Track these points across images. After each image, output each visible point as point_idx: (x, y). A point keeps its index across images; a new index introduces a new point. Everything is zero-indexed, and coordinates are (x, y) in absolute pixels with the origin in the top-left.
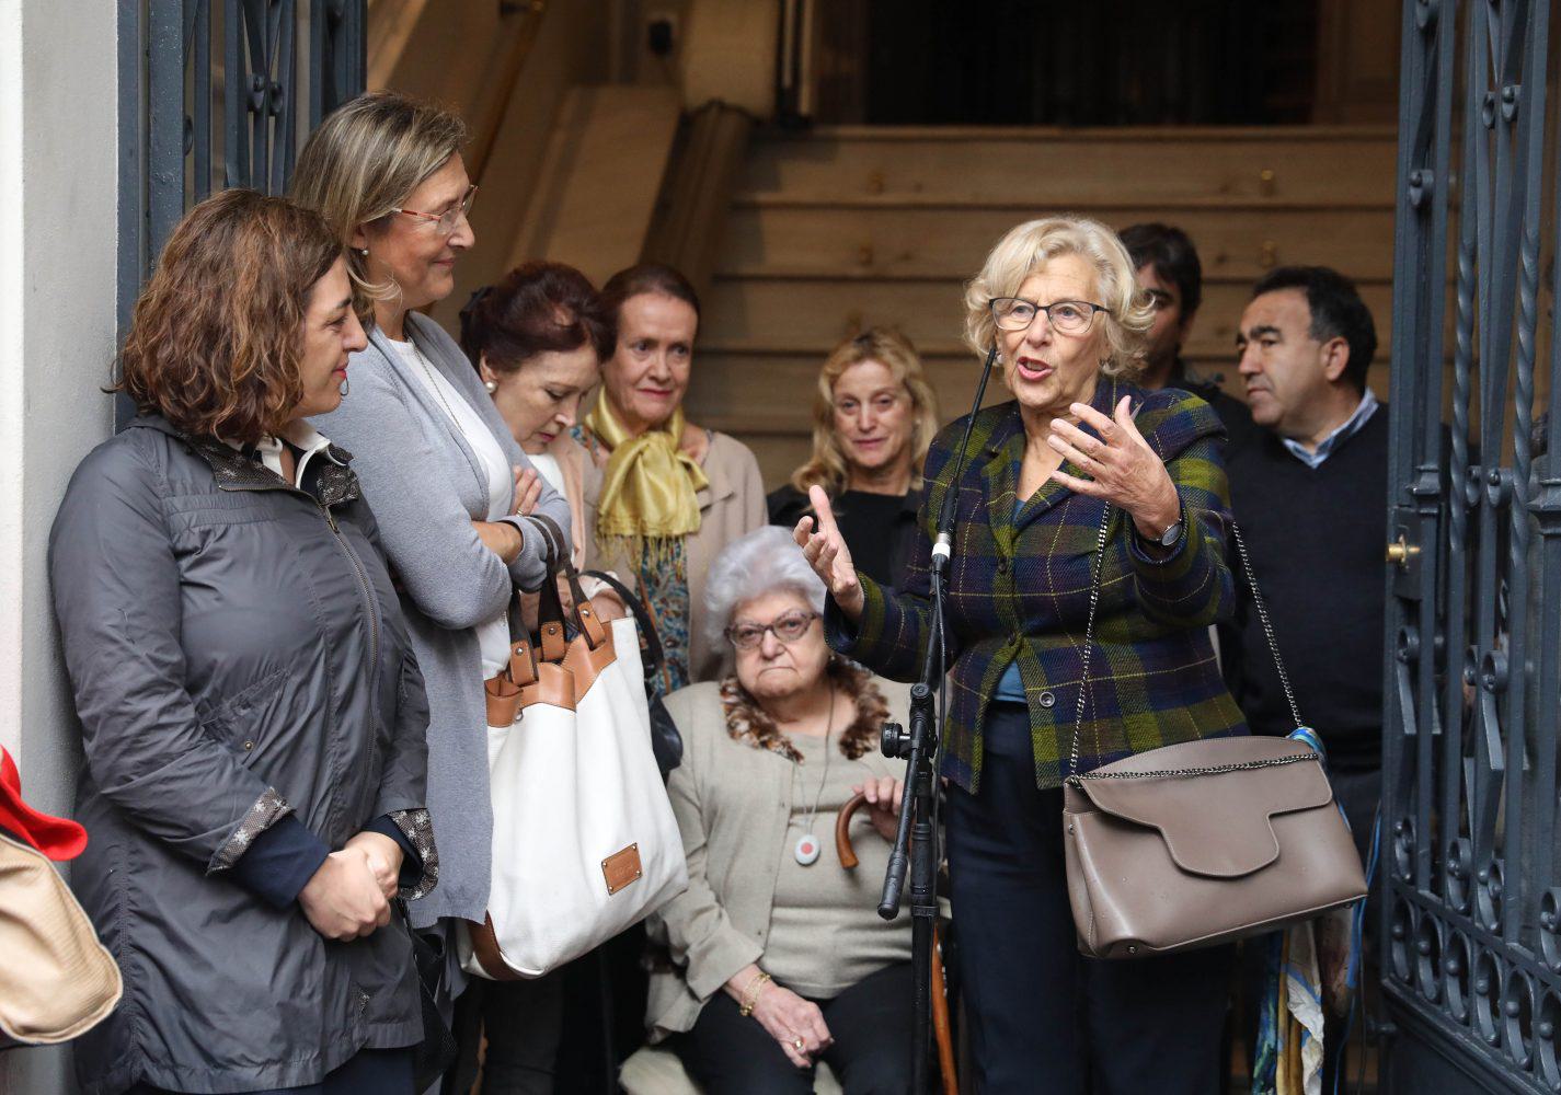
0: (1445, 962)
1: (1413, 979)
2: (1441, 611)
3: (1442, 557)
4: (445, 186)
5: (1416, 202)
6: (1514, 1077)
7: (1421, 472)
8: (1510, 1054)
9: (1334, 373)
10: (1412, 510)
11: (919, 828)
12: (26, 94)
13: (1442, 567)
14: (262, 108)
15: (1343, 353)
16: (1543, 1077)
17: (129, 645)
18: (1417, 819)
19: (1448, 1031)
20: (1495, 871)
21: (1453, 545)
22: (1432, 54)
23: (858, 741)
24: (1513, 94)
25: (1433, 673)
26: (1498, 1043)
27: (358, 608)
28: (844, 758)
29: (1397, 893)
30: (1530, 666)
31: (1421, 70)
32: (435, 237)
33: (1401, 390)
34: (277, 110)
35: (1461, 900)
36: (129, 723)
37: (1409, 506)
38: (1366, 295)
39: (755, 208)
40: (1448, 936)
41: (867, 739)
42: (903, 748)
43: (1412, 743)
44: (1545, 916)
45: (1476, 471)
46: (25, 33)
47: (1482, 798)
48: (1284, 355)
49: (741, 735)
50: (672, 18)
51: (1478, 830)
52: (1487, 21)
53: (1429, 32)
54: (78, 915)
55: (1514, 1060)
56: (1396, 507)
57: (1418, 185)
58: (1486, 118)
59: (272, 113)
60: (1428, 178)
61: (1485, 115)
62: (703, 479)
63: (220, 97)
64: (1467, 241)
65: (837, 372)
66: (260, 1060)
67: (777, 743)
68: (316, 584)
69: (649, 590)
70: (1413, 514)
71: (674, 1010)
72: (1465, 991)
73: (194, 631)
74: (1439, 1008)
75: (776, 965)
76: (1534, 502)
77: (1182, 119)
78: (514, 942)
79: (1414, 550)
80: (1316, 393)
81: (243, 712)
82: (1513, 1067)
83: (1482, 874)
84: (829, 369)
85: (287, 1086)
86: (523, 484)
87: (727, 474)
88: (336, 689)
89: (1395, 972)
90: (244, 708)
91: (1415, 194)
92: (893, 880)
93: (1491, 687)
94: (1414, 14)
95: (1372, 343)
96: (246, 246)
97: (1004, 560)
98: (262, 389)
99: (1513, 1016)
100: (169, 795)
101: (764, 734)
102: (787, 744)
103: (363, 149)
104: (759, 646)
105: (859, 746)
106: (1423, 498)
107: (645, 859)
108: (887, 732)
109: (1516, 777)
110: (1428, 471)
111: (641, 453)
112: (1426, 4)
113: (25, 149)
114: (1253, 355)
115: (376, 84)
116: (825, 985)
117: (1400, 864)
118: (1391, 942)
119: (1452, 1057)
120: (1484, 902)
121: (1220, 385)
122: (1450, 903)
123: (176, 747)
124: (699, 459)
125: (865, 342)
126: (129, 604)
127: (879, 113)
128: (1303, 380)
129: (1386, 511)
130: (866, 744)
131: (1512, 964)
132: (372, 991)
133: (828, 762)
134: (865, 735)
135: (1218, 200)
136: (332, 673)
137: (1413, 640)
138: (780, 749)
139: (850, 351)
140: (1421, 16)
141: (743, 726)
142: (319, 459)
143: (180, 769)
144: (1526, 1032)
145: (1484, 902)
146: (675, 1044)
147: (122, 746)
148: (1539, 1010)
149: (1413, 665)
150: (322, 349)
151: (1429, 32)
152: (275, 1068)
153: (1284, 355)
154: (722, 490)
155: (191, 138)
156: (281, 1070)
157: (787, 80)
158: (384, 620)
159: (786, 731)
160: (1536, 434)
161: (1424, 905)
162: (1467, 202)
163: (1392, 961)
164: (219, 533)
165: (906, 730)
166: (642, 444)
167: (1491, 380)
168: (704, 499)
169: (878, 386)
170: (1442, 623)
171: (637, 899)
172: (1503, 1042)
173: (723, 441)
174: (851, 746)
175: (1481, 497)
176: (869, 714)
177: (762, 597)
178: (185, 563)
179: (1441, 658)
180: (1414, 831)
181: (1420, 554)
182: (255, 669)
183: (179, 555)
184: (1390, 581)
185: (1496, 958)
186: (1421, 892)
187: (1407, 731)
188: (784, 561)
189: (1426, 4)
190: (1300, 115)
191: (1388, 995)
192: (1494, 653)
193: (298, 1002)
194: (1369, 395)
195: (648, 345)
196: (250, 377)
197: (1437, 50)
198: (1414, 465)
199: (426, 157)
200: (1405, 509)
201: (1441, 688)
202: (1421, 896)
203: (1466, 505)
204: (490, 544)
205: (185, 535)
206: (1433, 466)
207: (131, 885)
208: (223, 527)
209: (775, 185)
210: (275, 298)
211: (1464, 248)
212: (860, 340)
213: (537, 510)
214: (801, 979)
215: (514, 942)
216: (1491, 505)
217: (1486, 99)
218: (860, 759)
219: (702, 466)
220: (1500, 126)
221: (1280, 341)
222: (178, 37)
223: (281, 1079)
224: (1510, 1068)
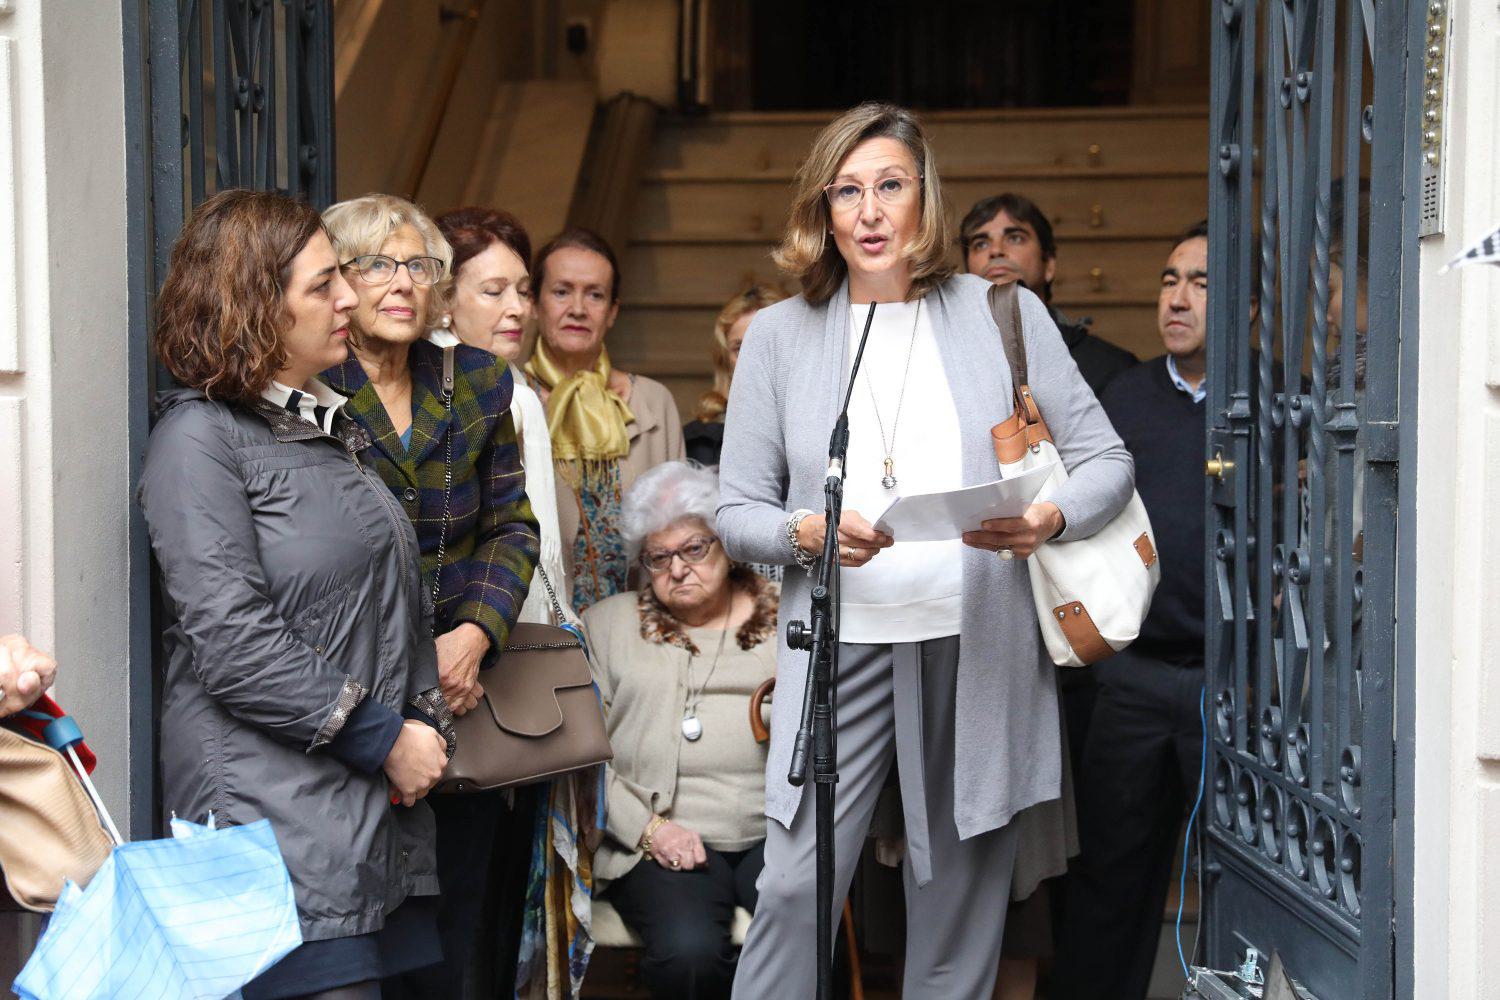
0: (1261, 811)
2: (1252, 515)
3: (1253, 469)
5: (1226, 172)
6: (1320, 905)
7: (1234, 399)
8: (1317, 886)
10: (1227, 432)
11: (820, 708)
12: (47, 99)
13: (1252, 479)
14: (247, 107)
16: (1345, 905)
17: (229, 570)
18: (1235, 690)
19: (1264, 868)
20: (1301, 733)
21: (1262, 460)
22: (1237, 45)
23: (751, 634)
24: (1306, 79)
25: (1249, 572)
26: (1306, 878)
27: (392, 534)
28: (739, 649)
29: (1219, 753)
31: (1228, 60)
33: (1215, 330)
34: (260, 108)
35: (1274, 758)
36: (237, 634)
37: (1224, 428)
39: (664, 183)
40: (1263, 789)
41: (759, 633)
42: (806, 641)
43: (1230, 627)
44: (1344, 770)
45: (1280, 397)
46: (44, 46)
47: (1290, 673)
49: (651, 634)
50: (587, 22)
51: (1287, 699)
52: (1283, 18)
53: (1234, 29)
54: (77, 790)
55: (1320, 891)
56: (1213, 429)
57: (1227, 157)
58: (1283, 100)
59: (255, 110)
61: (1283, 98)
62: (630, 415)
65: (730, 322)
66: (343, 911)
67: (678, 639)
68: (361, 515)
69: (592, 510)
70: (1228, 434)
73: (269, 557)
74: (1256, 850)
76: (1330, 423)
77: (1020, 102)
79: (1229, 465)
81: (314, 622)
82: (1320, 897)
83: (1291, 736)
84: (723, 320)
85: (364, 932)
87: (650, 407)
88: (381, 600)
89: (1219, 820)
90: (314, 619)
91: (1225, 165)
92: (800, 753)
93: (1296, 579)
94: (1221, 12)
99: (1319, 854)
100: (276, 688)
104: (669, 569)
105: (752, 638)
106: (1237, 421)
108: (792, 628)
109: (1319, 656)
110: (1240, 398)
111: (577, 389)
112: (1231, 4)
113: (46, 146)
117: (1222, 729)
118: (1214, 795)
119: (1268, 890)
121: (1088, 327)
122: (1264, 761)
123: (277, 649)
124: (626, 398)
125: (752, 296)
126: (223, 538)
127: (762, 104)
129: (1204, 432)
130: (758, 637)
131: (1317, 811)
132: (409, 849)
133: (721, 651)
134: (757, 629)
135: (1056, 171)
136: (377, 587)
137: (1229, 541)
138: (680, 643)
139: (740, 304)
140: (1227, 14)
141: (652, 627)
143: (283, 665)
144: (1330, 867)
145: (1293, 759)
147: (234, 653)
148: (1341, 850)
149: (1230, 562)
151: (1234, 29)
152: (354, 918)
155: (188, 134)
156: (359, 920)
157: (687, 74)
158: (409, 543)
161: (1242, 763)
162: (1268, 169)
163: (1216, 811)
164: (282, 477)
165: (808, 625)
166: (577, 382)
167: (1292, 320)
168: (632, 431)
170: (1254, 527)
172: (1311, 874)
173: (644, 383)
176: (763, 612)
177: (669, 529)
178: (256, 501)
179: (1253, 555)
180: (1233, 702)
181: (1233, 469)
182: (324, 586)
183: (251, 495)
184: (1209, 491)
185: (1304, 806)
186: (1239, 752)
187: (1226, 617)
188: (684, 496)
189: (1231, 4)
190: (1120, 97)
191: (1212, 837)
192: (1298, 551)
193: (372, 864)
195: (568, 287)
197: (1241, 44)
198: (1227, 393)
200: (1220, 431)
202: (1240, 756)
203: (1272, 426)
205: (255, 480)
206: (1244, 394)
208: (284, 472)
209: (678, 164)
210: (254, 276)
211: (1267, 210)
212: (748, 295)
214: (715, 838)
216: (1294, 427)
217: (1283, 83)
218: (752, 650)
219: (628, 403)
220: (1296, 107)
222: (174, 47)
223: (359, 928)
224: (1317, 898)
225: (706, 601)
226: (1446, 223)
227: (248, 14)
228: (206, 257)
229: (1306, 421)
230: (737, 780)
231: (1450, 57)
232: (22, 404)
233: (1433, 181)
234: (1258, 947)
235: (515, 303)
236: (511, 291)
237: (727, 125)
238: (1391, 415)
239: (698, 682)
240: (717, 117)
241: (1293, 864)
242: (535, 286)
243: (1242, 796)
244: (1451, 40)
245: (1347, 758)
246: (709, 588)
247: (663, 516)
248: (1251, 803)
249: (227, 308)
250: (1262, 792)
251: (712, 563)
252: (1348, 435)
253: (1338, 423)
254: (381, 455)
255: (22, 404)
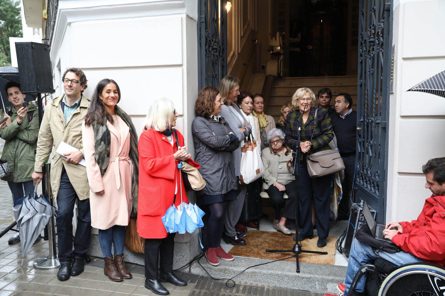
1: (360, 182)
4: (237, 88)
9: (347, 107)
15: (348, 104)
20: (370, 169)
25: (363, 145)
30: (375, 143)
32: (235, 94)
38: (351, 97)
43: (360, 153)
44: (377, 174)
48: (340, 104)
50: (265, 65)
53: (361, 63)
57: (360, 82)
58: (369, 73)
60: (362, 81)
62: (267, 120)
63: (210, 76)
64: (367, 89)
71: (266, 187)
72: (366, 184)
75: (278, 181)
78: (245, 180)
80: (345, 109)
82: (373, 193)
86: (246, 123)
87: (270, 120)
91: (360, 83)
95: (352, 103)
96: (207, 92)
97: (304, 131)
98: (209, 109)
101: (275, 153)
102: (278, 154)
103: (228, 84)
106: (361, 122)
107: (260, 170)
114: (337, 104)
115: (228, 74)
116: (285, 183)
120: (369, 172)
128: (343, 108)
133: (283, 156)
135: (335, 85)
137: (360, 140)
141: (273, 152)
142: (220, 119)
145: (369, 172)
146: (266, 191)
149: (360, 143)
150: (218, 104)
151: (361, 63)
153: (340, 104)
154: (270, 122)
157: (279, 72)
159: (278, 153)
160: (376, 114)
161: (361, 173)
169: (288, 110)
170: (364, 138)
171: (259, 175)
174: (286, 154)
175: (369, 121)
177: (274, 138)
179: (364, 142)
181: (361, 129)
188: (276, 133)
194: (351, 109)
196: (207, 108)
199: (235, 84)
201: (364, 146)
203: (367, 122)
204: (242, 131)
207: (203, 168)
210: (211, 98)
213: (248, 126)
215: (245, 180)
220: (371, 74)
221: (340, 102)
225: (280, 149)
226: (394, 91)
227: (215, 64)
228: (203, 95)
229: (372, 122)
230: (286, 175)
231: (394, 70)
232: (183, 119)
233: (392, 85)
234: (363, 200)
235: (250, 105)
236: (250, 103)
237: (285, 79)
238: (385, 121)
239: (281, 161)
240: (284, 78)
241: (369, 188)
242: (253, 103)
243: (361, 178)
244: (395, 64)
245: (377, 172)
246: (280, 147)
247: (273, 136)
248: (363, 179)
249: (206, 102)
250: (364, 177)
251: (280, 143)
252: (379, 123)
253: (377, 122)
254: (46, 96)
255: (183, 119)
